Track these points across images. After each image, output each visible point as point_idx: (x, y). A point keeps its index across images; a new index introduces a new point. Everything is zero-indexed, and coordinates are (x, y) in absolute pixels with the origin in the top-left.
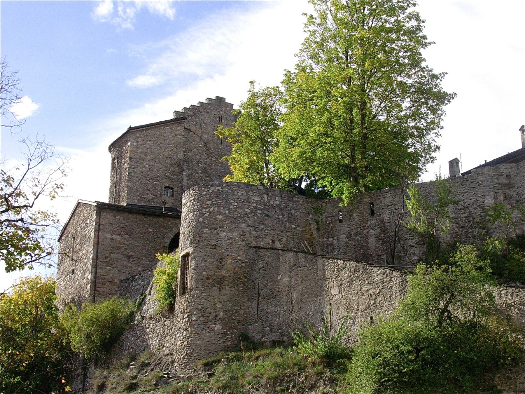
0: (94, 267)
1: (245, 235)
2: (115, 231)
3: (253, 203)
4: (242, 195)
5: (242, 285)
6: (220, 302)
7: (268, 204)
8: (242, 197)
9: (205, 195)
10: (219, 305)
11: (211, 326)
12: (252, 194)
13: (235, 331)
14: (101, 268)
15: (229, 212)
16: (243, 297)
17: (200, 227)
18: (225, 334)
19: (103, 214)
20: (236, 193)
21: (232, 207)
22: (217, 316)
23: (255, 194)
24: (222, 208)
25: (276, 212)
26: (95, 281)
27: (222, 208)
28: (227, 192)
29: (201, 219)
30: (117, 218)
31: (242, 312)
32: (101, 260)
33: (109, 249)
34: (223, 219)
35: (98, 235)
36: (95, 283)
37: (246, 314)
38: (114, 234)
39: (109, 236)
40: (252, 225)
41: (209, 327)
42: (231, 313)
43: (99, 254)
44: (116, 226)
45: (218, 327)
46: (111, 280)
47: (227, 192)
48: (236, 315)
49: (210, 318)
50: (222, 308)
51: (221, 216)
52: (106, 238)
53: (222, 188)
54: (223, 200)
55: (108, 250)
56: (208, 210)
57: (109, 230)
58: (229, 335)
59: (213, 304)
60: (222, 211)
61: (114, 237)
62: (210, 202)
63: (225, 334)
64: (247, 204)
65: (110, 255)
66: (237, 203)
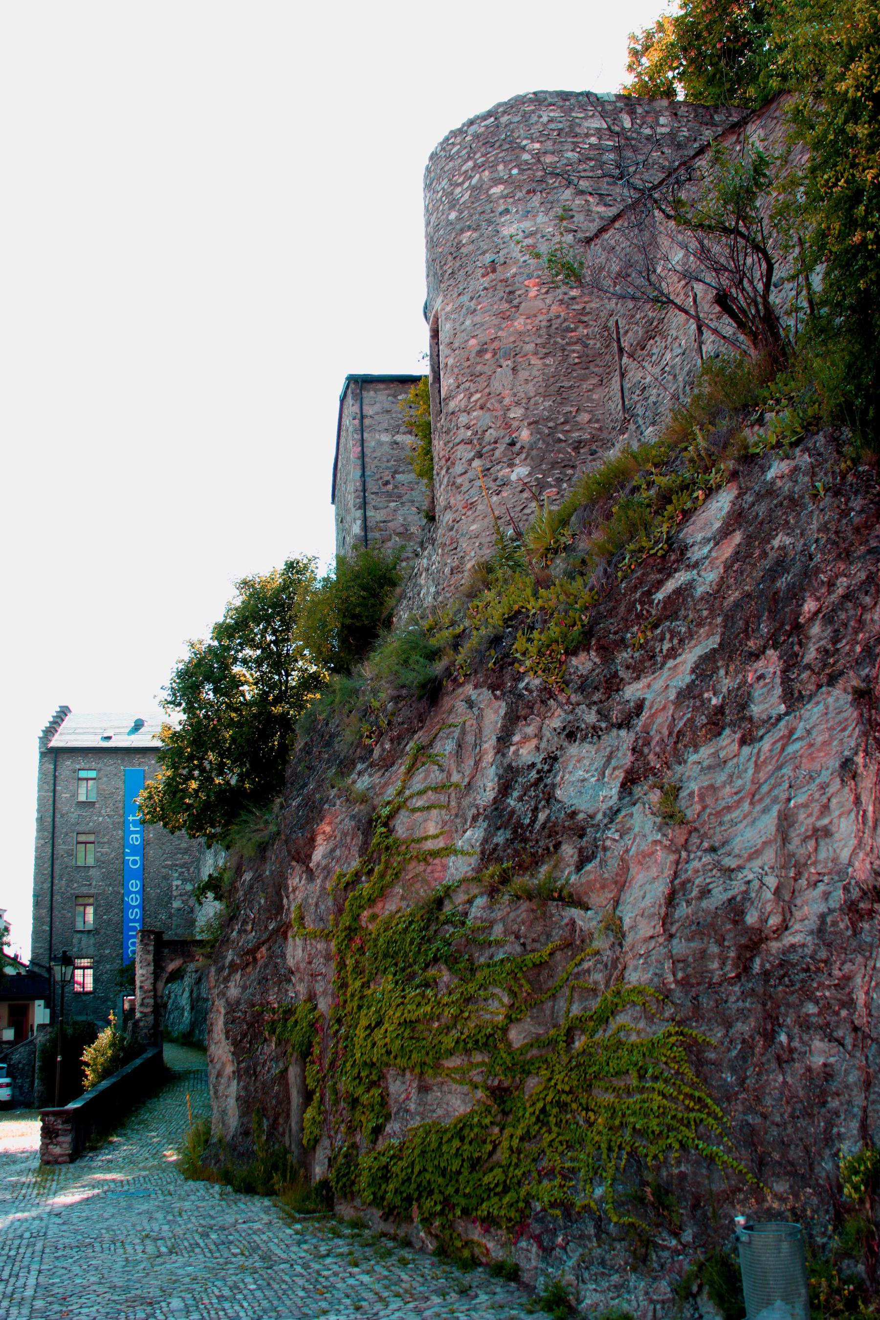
0: (360, 508)
1: (572, 217)
2: (399, 426)
3: (587, 135)
4: (551, 120)
5: (577, 347)
6: (518, 403)
7: (634, 135)
8: (552, 126)
9: (458, 152)
10: (516, 413)
11: (500, 474)
12: (582, 115)
13: (570, 472)
14: (376, 508)
15: (522, 171)
16: (584, 379)
17: (453, 235)
18: (542, 486)
19: (369, 395)
20: (534, 118)
21: (526, 156)
22: (512, 444)
23: (591, 113)
24: (501, 167)
25: (663, 153)
26: (366, 536)
27: (501, 167)
28: (511, 123)
29: (453, 216)
30: (400, 397)
31: (584, 417)
32: (374, 490)
33: (389, 464)
34: (506, 192)
35: (363, 440)
36: (366, 540)
37: (597, 421)
38: (398, 433)
39: (385, 438)
40: (590, 190)
41: (495, 480)
42: (551, 424)
43: (368, 479)
44: (400, 416)
45: (521, 471)
46: (401, 530)
47: (511, 123)
48: (567, 428)
49: (497, 453)
50: (525, 417)
51: (501, 187)
52: (380, 444)
53: (496, 119)
54: (501, 146)
55: (387, 468)
56: (466, 185)
57: (385, 426)
58: (551, 486)
59: (500, 413)
60: (501, 175)
61: (399, 438)
62: (470, 164)
63: (542, 486)
64: (570, 140)
65: (393, 477)
66: (541, 142)
